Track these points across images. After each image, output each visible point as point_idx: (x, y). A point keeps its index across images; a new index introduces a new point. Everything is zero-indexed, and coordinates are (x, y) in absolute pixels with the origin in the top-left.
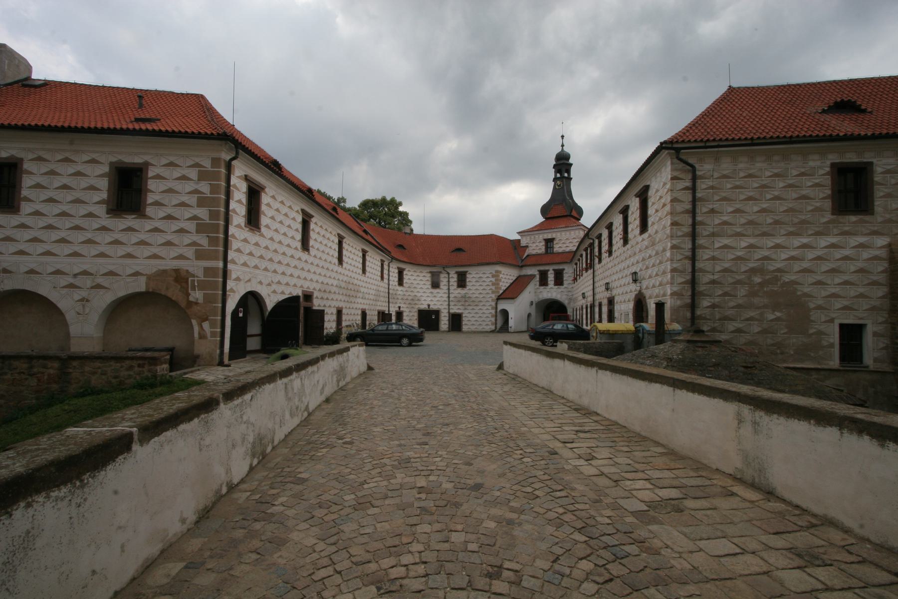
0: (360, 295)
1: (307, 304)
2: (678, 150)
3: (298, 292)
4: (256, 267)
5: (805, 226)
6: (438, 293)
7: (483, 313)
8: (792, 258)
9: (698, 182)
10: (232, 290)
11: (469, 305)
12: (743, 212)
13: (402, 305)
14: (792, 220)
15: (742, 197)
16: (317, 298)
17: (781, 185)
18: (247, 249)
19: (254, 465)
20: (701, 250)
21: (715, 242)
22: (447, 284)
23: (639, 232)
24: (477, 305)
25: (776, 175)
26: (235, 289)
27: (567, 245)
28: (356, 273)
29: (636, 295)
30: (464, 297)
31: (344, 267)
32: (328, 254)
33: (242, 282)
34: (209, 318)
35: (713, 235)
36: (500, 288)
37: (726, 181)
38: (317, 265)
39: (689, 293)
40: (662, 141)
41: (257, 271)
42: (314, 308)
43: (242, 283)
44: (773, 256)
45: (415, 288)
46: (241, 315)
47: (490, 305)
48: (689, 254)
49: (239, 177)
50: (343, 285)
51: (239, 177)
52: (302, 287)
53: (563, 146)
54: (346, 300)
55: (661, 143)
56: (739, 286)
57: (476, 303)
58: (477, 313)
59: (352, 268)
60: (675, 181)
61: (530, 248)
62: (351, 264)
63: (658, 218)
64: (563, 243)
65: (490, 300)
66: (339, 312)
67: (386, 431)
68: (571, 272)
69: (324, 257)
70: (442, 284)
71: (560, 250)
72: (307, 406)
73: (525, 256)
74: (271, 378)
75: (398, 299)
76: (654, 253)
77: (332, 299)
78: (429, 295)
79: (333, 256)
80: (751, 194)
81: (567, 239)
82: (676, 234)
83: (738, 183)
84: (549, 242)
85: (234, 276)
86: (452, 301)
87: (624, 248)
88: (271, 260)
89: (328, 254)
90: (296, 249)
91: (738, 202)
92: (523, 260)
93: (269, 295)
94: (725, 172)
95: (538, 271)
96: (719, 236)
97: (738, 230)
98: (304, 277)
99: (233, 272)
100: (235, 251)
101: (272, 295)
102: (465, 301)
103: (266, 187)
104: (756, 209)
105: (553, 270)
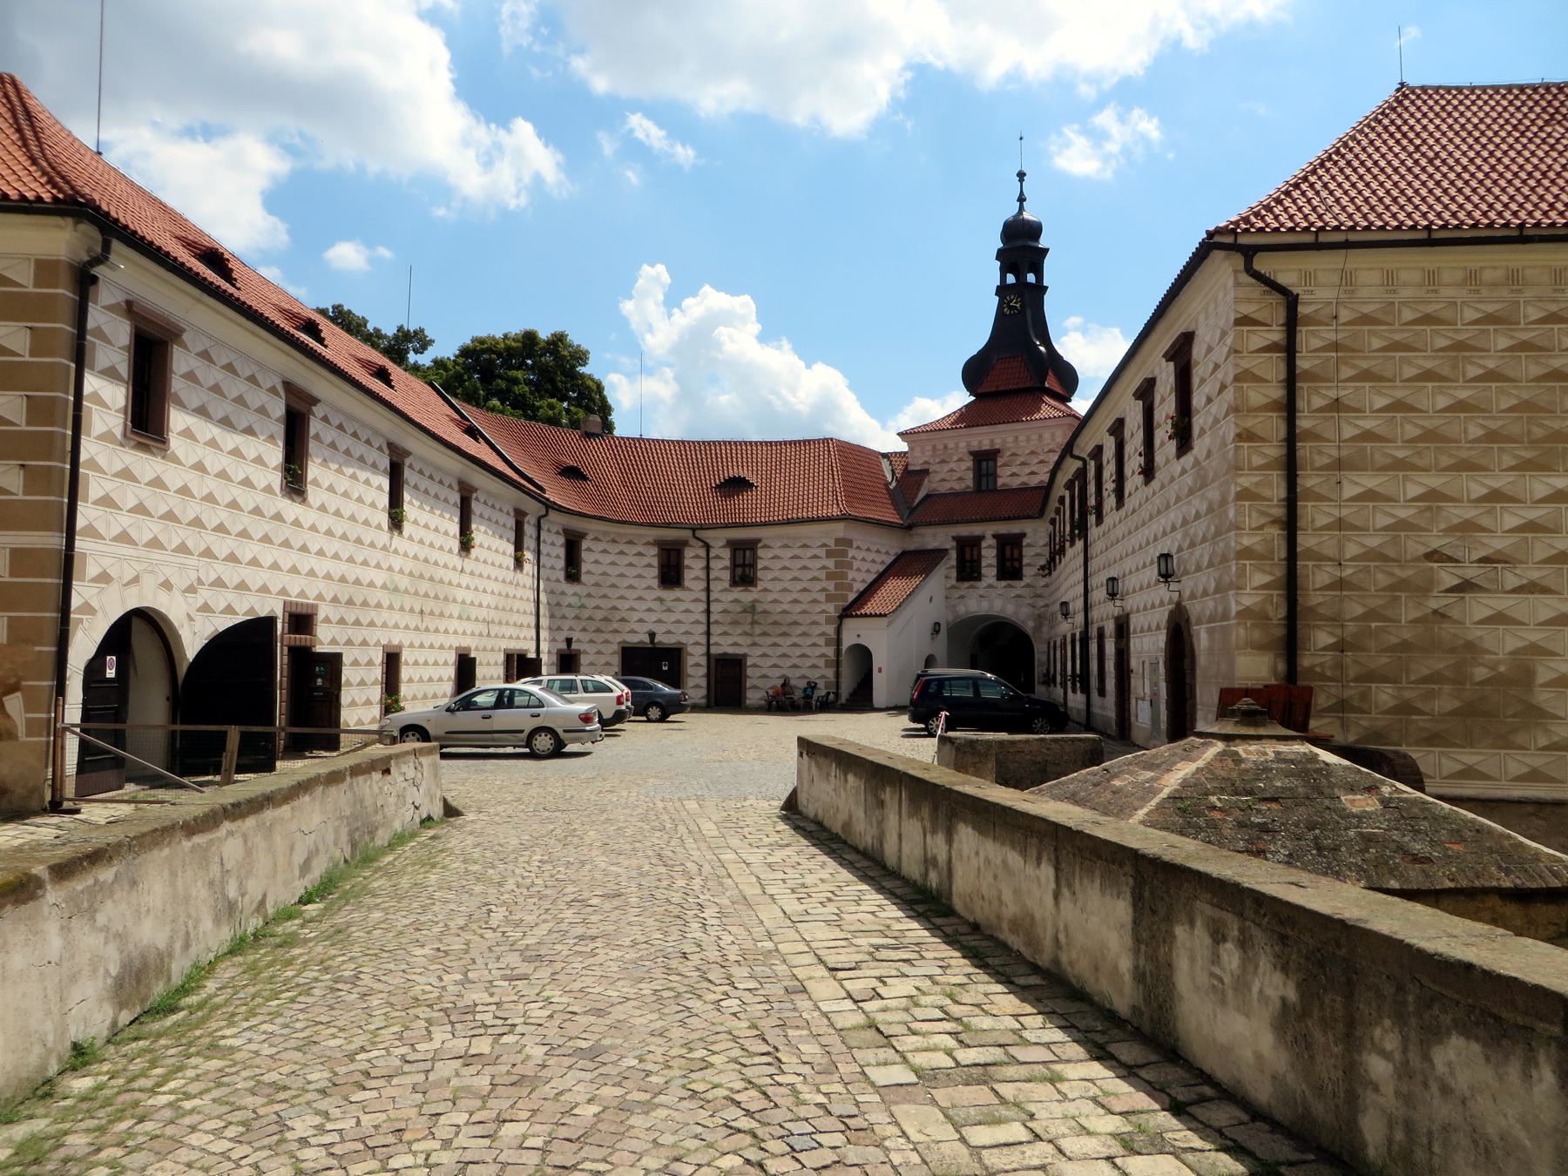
0: (455, 610)
1: (301, 639)
2: (1249, 252)
3: (271, 606)
4: (155, 543)
5: (1560, 446)
6: (678, 600)
7: (804, 656)
8: (1531, 527)
9: (1303, 332)
10: (88, 609)
11: (764, 634)
12: (1412, 409)
13: (575, 636)
14: (1529, 432)
15: (1409, 372)
16: (327, 620)
17: (1503, 342)
18: (129, 496)
19: (121, 1024)
20: (1310, 504)
21: (1345, 483)
22: (702, 574)
23: (1174, 450)
24: (784, 634)
25: (1490, 319)
26: (95, 604)
27: (1034, 469)
28: (441, 548)
29: (1171, 612)
30: (751, 609)
31: (406, 532)
32: (360, 500)
33: (115, 587)
34: (24, 683)
35: (1339, 465)
36: (850, 588)
37: (1369, 331)
38: (329, 533)
39: (1282, 612)
40: (1212, 228)
41: (156, 555)
42: (319, 649)
43: (114, 588)
44: (1486, 521)
45: (613, 586)
46: (111, 673)
47: (823, 634)
48: (1280, 512)
49: (110, 308)
50: (404, 582)
51: (110, 308)
52: (283, 591)
53: (1021, 199)
54: (412, 626)
55: (1210, 234)
56: (1403, 595)
57: (784, 629)
58: (784, 655)
59: (429, 537)
60: (1245, 328)
61: (935, 478)
62: (426, 526)
63: (1210, 420)
64: (1023, 464)
65: (821, 619)
66: (392, 661)
67: (442, 954)
68: (1042, 542)
69: (349, 508)
70: (688, 576)
71: (1015, 483)
72: (262, 903)
73: (917, 501)
74: (162, 834)
75: (564, 617)
76: (1204, 507)
77: (372, 624)
78: (655, 605)
79: (373, 505)
80: (1429, 365)
81: (1033, 453)
82: (1250, 461)
83: (1397, 337)
84: (985, 461)
85: (92, 570)
86: (717, 622)
87: (1146, 489)
88: (197, 523)
89: (360, 500)
90: (268, 489)
91: (1398, 383)
92: (912, 510)
93: (190, 619)
94: (1367, 309)
95: (954, 538)
96: (1354, 467)
97: (1400, 454)
98: (289, 566)
99: (90, 561)
100: (96, 503)
101: (199, 617)
102: (753, 623)
103: (182, 331)
104: (1442, 401)
105: (994, 536)
